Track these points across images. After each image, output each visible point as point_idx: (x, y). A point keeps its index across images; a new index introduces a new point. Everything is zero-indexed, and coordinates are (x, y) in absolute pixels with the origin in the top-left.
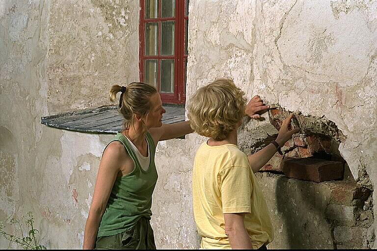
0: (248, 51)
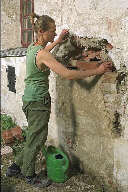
0: (59, 11)
